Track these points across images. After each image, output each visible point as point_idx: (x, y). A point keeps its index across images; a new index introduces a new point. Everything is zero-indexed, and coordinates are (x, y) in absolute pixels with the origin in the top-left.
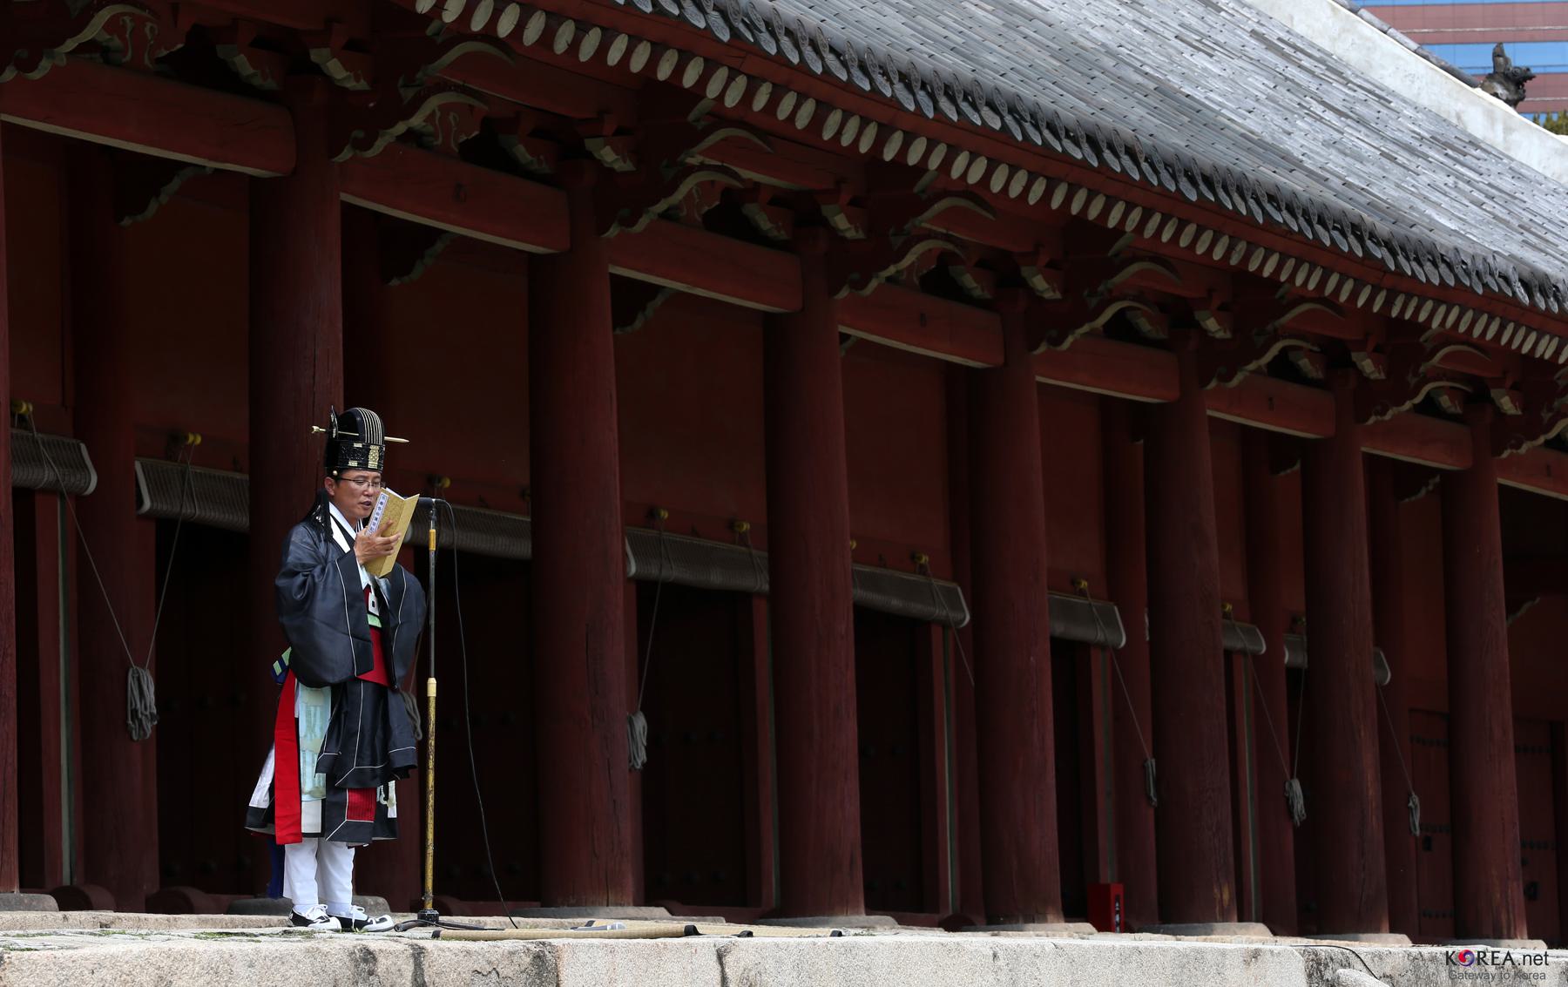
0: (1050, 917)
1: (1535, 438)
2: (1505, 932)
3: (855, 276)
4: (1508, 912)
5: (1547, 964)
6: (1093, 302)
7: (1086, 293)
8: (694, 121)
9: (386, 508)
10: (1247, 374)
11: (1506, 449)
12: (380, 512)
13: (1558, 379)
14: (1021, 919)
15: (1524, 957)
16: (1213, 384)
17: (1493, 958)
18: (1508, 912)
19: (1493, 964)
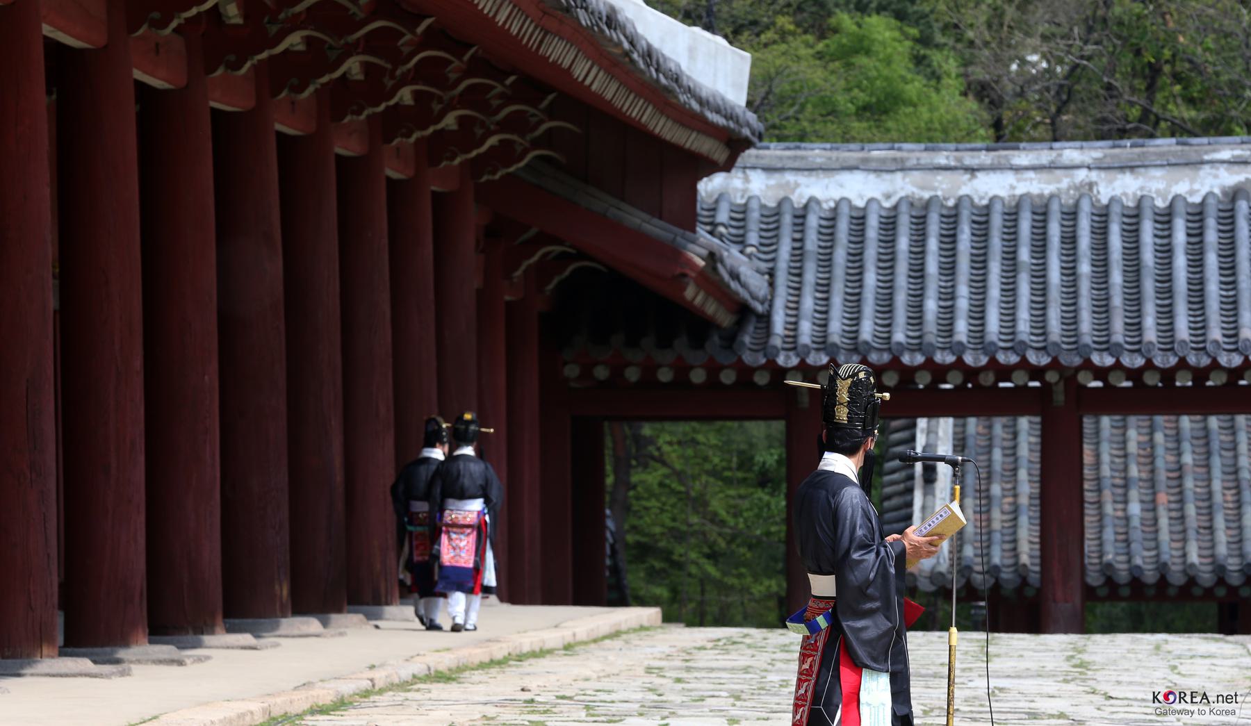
0: (218, 629)
1: (425, 128)
2: (383, 599)
3: (156, 15)
4: (386, 580)
5: (1236, 703)
6: (274, 29)
7: (266, 20)
8: (862, 199)
9: (944, 521)
10: (319, 86)
11: (397, 137)
12: (936, 521)
13: (402, 45)
14: (191, 632)
15: (1218, 696)
16: (220, 72)
17: (1192, 697)
18: (386, 580)
19: (1192, 702)
